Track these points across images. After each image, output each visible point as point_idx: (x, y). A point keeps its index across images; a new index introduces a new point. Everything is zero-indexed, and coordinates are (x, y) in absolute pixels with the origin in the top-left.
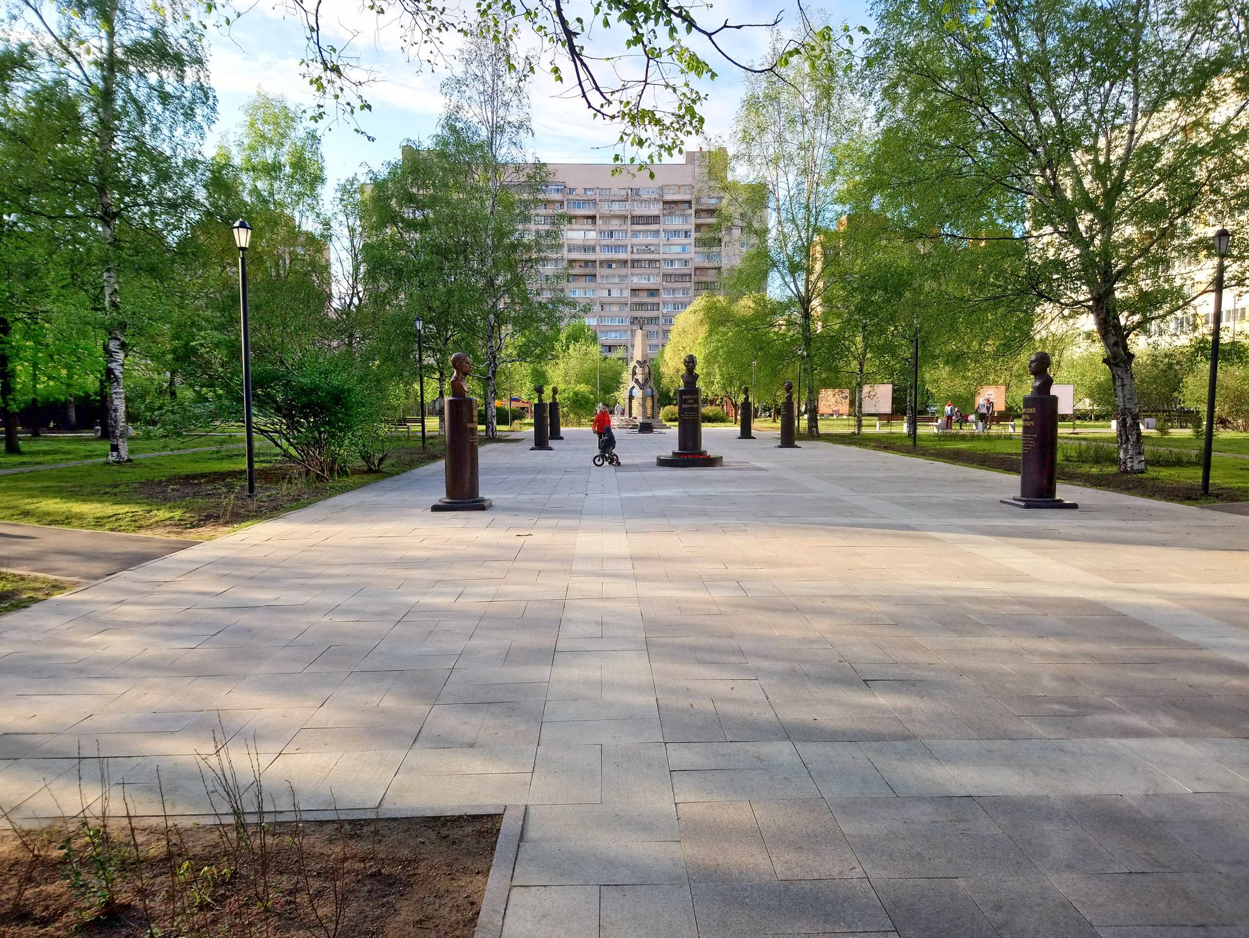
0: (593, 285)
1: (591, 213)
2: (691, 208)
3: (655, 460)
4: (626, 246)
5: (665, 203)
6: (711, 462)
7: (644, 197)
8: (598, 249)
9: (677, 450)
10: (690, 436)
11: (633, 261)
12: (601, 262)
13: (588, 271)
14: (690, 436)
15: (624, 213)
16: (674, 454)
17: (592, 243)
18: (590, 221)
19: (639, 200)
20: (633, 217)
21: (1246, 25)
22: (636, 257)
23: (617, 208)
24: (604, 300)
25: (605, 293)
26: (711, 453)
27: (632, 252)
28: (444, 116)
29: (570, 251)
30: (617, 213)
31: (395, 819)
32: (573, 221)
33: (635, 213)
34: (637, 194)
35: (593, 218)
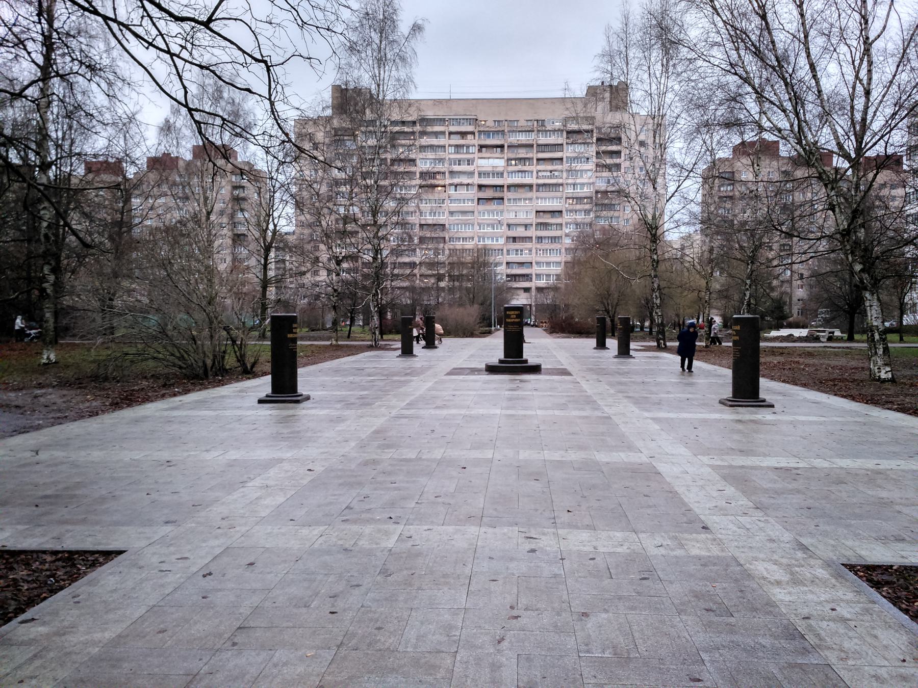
0: (501, 207)
1: (499, 142)
2: (592, 136)
3: (484, 367)
4: (532, 172)
5: (568, 132)
6: (536, 369)
7: (549, 128)
8: (505, 174)
9: (502, 357)
10: (514, 345)
11: (538, 185)
12: (509, 187)
13: (498, 195)
14: (514, 345)
15: (531, 142)
16: (501, 361)
17: (501, 169)
18: (499, 149)
19: (546, 131)
20: (538, 145)
21: (2, 180)
22: (541, 181)
23: (523, 138)
24: (511, 222)
25: (512, 215)
26: (532, 361)
27: (537, 178)
28: (414, 66)
29: (480, 176)
30: (524, 142)
31: (23, 433)
32: (484, 149)
33: (540, 142)
34: (543, 125)
35: (502, 147)
